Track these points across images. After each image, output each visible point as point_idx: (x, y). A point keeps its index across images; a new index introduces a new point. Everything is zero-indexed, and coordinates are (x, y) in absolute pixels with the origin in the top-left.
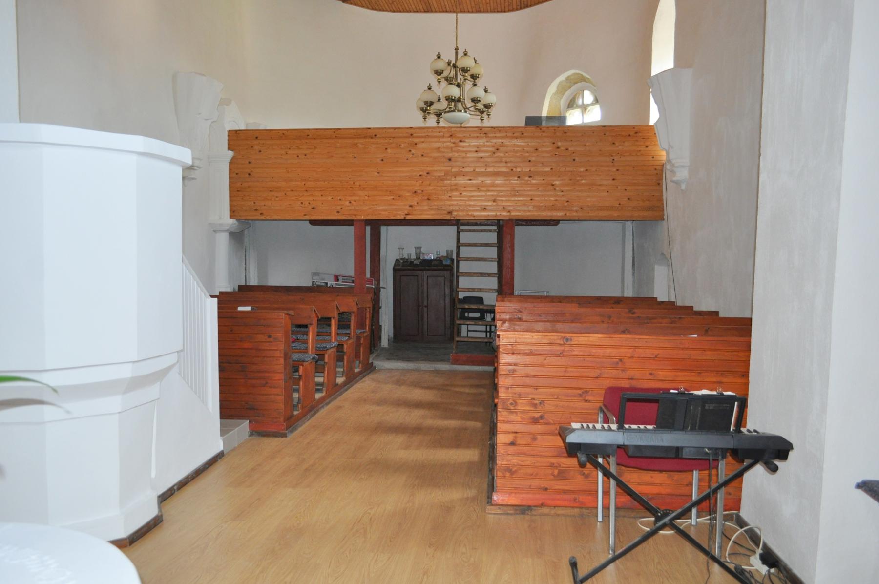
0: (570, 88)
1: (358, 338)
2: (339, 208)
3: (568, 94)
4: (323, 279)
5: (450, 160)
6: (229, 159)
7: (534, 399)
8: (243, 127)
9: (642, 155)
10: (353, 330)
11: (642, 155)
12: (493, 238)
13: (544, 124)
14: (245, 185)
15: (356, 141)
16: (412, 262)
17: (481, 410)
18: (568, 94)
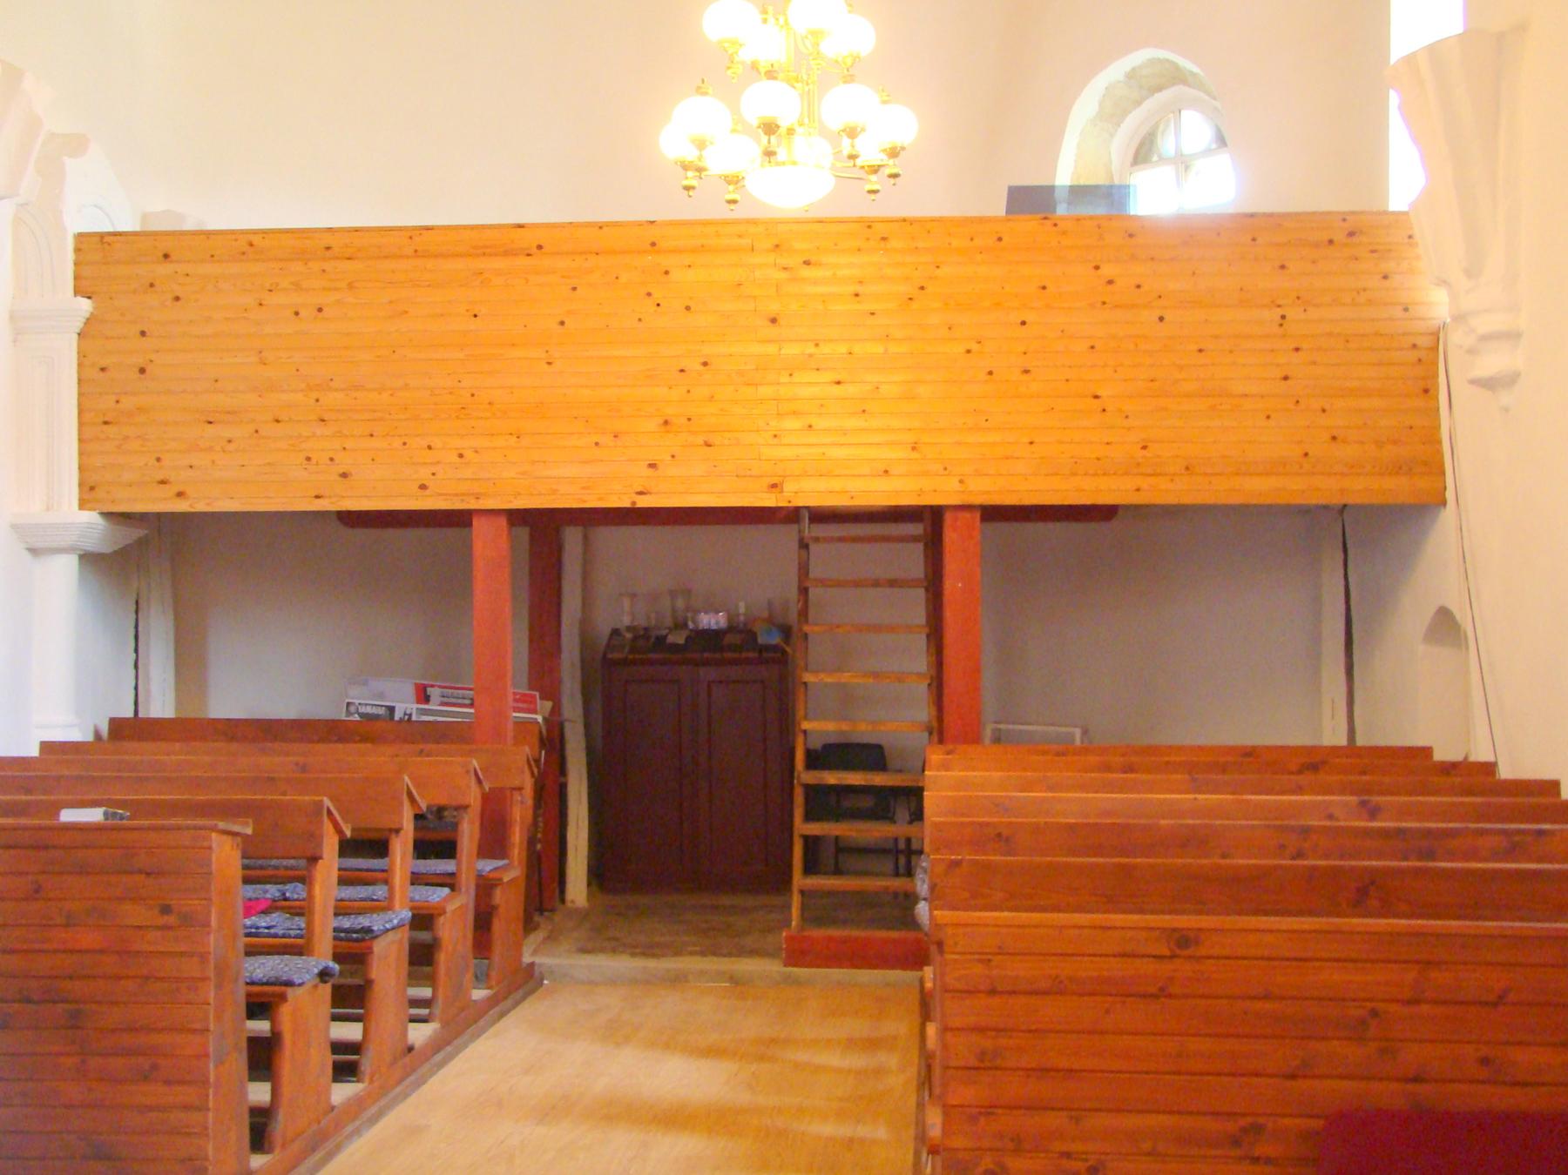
0: (1139, 103)
1: (486, 887)
2: (424, 474)
3: (1133, 122)
4: (381, 696)
5: (774, 321)
6: (79, 324)
7: (1067, 1155)
8: (127, 223)
9: (1370, 302)
10: (470, 863)
11: (1370, 302)
12: (912, 561)
13: (1062, 210)
14: (128, 403)
15: (481, 264)
16: (661, 640)
17: (882, 1133)
18: (1133, 122)
